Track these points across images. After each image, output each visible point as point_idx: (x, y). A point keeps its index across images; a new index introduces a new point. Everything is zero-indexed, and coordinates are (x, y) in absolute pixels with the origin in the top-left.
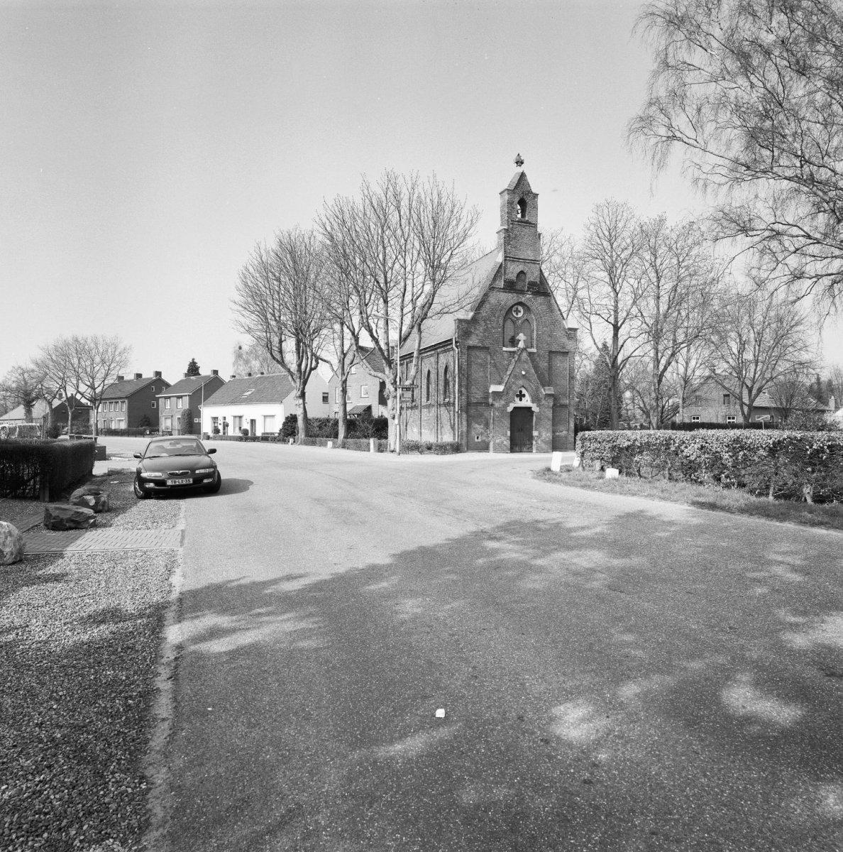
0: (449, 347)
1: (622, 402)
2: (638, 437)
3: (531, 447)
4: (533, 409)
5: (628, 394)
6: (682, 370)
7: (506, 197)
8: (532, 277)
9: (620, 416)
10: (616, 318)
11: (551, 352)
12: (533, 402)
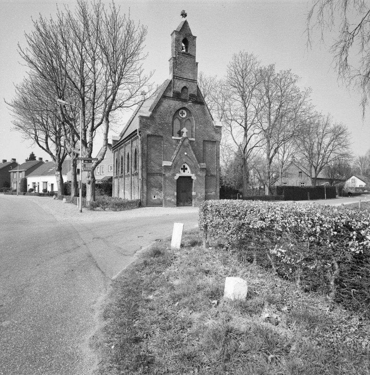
0: (136, 136)
1: (249, 175)
2: (279, 218)
3: (191, 203)
4: (192, 178)
5: (251, 172)
6: (281, 157)
7: (175, 36)
8: (192, 90)
9: (248, 182)
10: (246, 124)
11: (204, 141)
12: (192, 172)
